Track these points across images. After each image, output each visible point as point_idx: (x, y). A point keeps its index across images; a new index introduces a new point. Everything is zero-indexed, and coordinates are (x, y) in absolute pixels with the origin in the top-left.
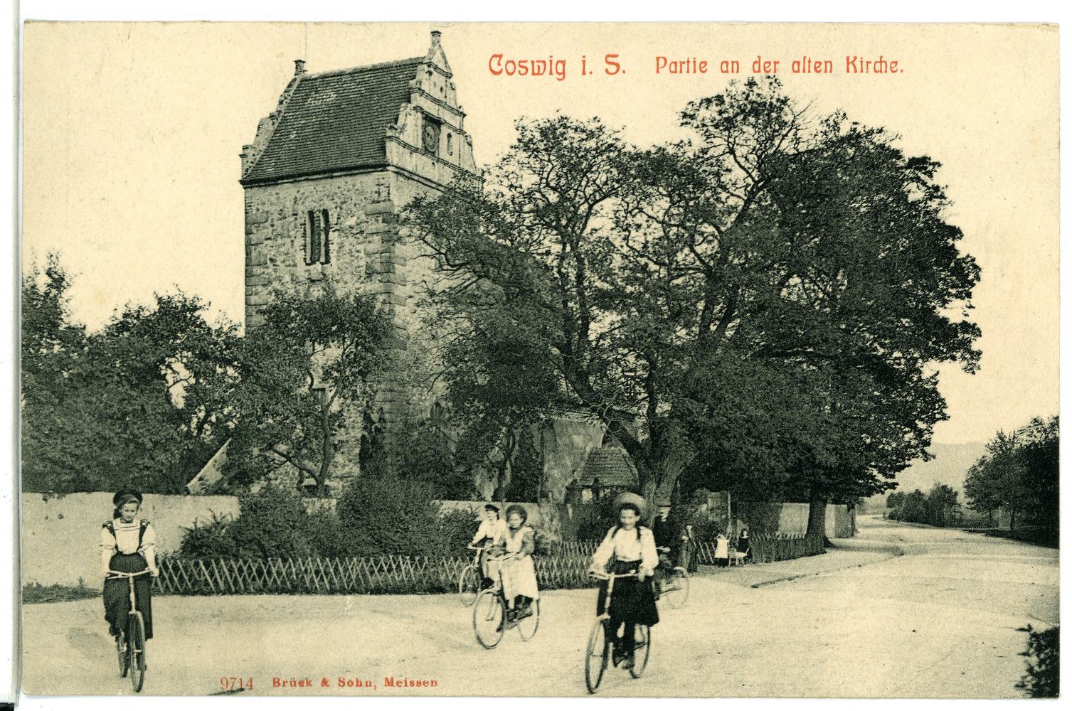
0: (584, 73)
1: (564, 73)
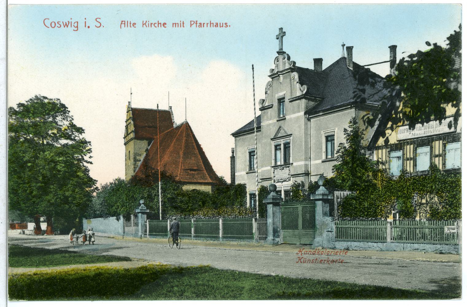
0: (85, 26)
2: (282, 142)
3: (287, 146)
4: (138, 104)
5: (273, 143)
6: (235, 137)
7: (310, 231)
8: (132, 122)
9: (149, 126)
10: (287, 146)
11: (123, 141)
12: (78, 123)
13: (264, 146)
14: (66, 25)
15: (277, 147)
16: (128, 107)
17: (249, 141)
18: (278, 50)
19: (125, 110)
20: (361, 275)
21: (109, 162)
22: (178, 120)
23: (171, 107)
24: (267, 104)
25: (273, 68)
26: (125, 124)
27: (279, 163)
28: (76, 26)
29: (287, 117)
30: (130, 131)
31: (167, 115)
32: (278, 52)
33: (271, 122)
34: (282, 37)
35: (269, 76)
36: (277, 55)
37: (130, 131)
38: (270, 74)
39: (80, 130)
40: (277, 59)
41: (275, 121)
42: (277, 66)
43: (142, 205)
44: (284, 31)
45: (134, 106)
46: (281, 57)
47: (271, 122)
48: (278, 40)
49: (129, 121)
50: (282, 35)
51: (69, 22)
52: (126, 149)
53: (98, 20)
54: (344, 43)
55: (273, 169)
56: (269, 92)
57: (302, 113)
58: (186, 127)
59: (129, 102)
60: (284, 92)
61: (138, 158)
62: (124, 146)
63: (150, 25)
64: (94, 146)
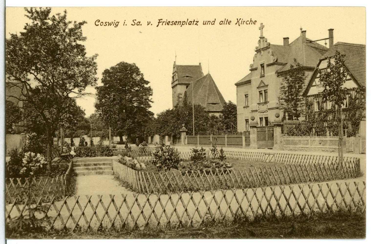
1: (117, 25)
2: (263, 89)
3: (266, 91)
4: (180, 62)
5: (258, 90)
6: (237, 86)
7: (270, 142)
8: (177, 74)
9: (188, 77)
10: (266, 92)
11: (171, 86)
12: (146, 79)
13: (253, 91)
14: (110, 24)
15: (261, 94)
16: (174, 65)
17: (244, 89)
18: (260, 36)
19: (172, 67)
20: (17, 85)
21: (161, 101)
22: (205, 72)
23: (200, 64)
24: (254, 67)
25: (258, 46)
26: (172, 75)
27: (261, 102)
28: (117, 24)
29: (265, 75)
30: (175, 80)
31: (198, 68)
32: (260, 38)
33: (256, 77)
34: (262, 28)
35: (256, 51)
36: (259, 39)
37: (175, 80)
38: (256, 50)
39: (147, 83)
40: (260, 41)
41: (259, 77)
42: (260, 45)
43: (184, 127)
44: (263, 25)
45: (178, 64)
46: (262, 40)
47: (256, 77)
48: (260, 30)
49: (175, 74)
50: (262, 27)
51: (112, 22)
52: (173, 91)
53: (134, 21)
54: (302, 28)
55: (258, 105)
56: (255, 60)
57: (274, 73)
58: (209, 76)
59: (175, 62)
60: (264, 61)
61: (180, 96)
62: (172, 88)
63: (243, 22)
64: (154, 92)
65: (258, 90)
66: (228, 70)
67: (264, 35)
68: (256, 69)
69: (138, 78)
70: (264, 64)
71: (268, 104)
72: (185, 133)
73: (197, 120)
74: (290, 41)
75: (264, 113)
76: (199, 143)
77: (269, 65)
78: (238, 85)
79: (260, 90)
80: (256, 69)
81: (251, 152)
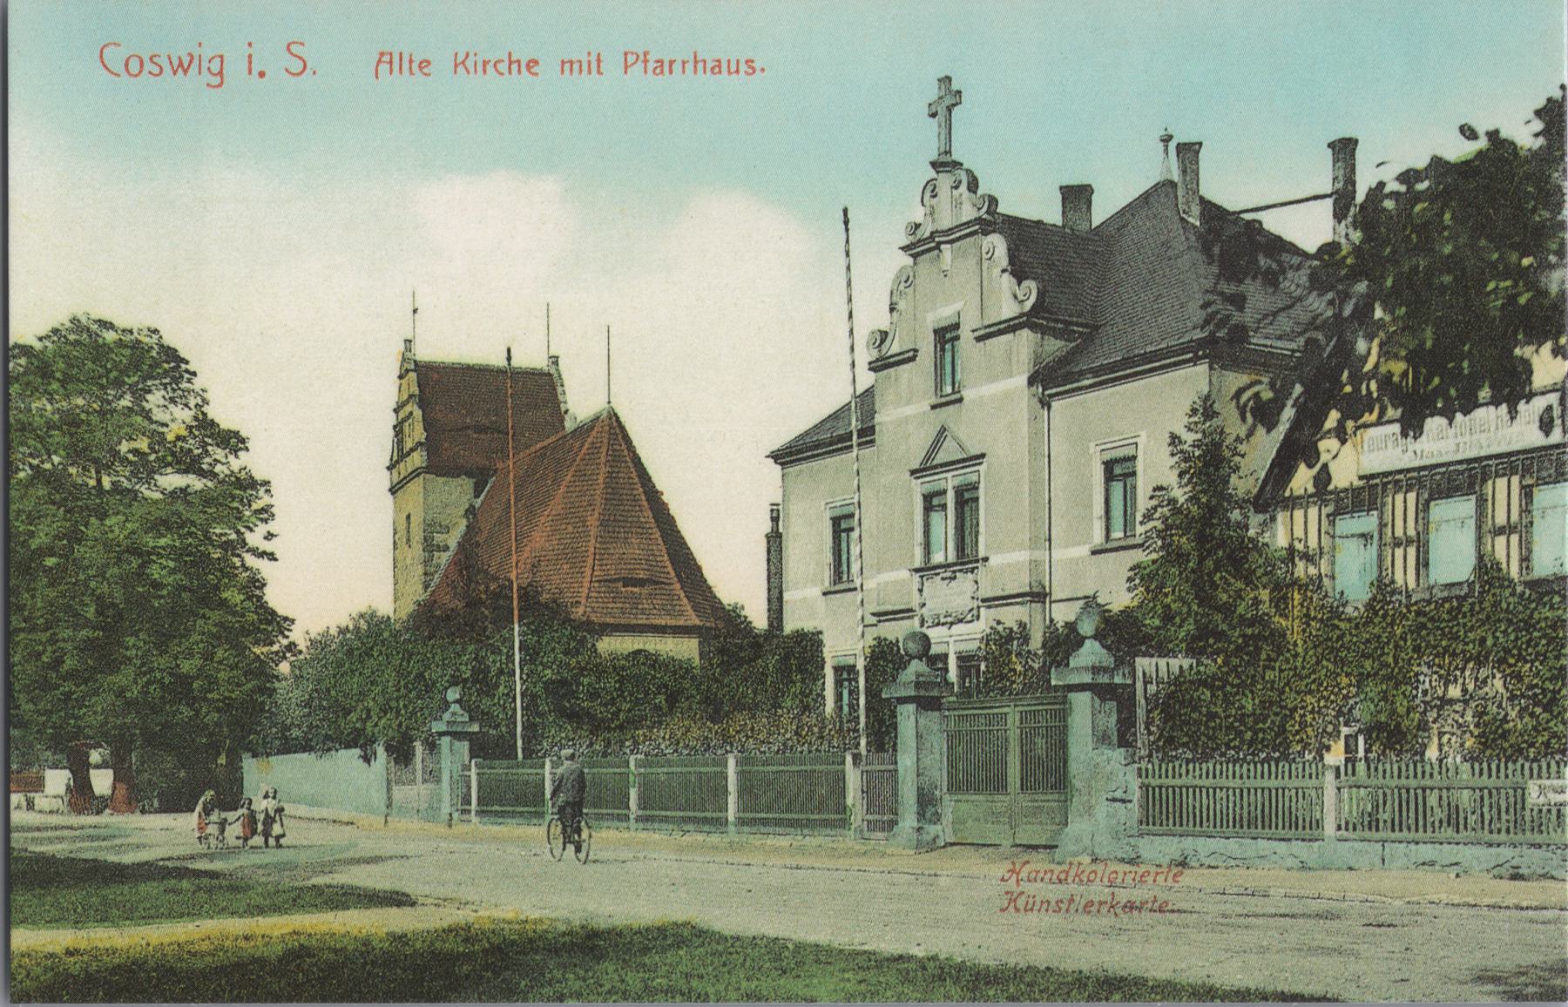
4: (439, 348)
5: (918, 488)
7: (1050, 800)
8: (418, 413)
9: (478, 426)
10: (966, 499)
11: (384, 480)
12: (224, 414)
15: (931, 502)
16: (404, 360)
17: (832, 478)
19: (394, 369)
23: (555, 360)
24: (895, 349)
27: (938, 558)
30: (409, 444)
33: (909, 411)
34: (949, 109)
37: (409, 444)
38: (905, 242)
39: (234, 441)
40: (931, 189)
43: (455, 708)
44: (955, 87)
45: (426, 352)
46: (945, 181)
49: (408, 408)
50: (948, 101)
52: (397, 509)
56: (901, 305)
65: (918, 488)
66: (728, 361)
67: (956, 156)
68: (910, 357)
69: (177, 419)
70: (957, 326)
71: (982, 573)
72: (464, 747)
73: (533, 661)
74: (1102, 210)
75: (957, 629)
76: (743, 807)
77: (985, 335)
78: (786, 456)
79: (928, 488)
80: (910, 357)
81: (1039, 885)
